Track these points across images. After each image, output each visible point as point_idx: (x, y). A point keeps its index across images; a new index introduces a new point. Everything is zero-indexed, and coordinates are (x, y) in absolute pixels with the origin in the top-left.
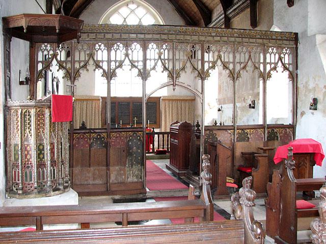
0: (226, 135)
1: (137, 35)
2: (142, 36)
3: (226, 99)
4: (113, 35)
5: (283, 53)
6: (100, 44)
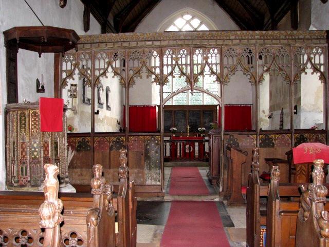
0: (248, 140)
1: (153, 43)
2: (158, 43)
3: (275, 106)
4: (129, 43)
5: (313, 53)
6: (184, 50)
